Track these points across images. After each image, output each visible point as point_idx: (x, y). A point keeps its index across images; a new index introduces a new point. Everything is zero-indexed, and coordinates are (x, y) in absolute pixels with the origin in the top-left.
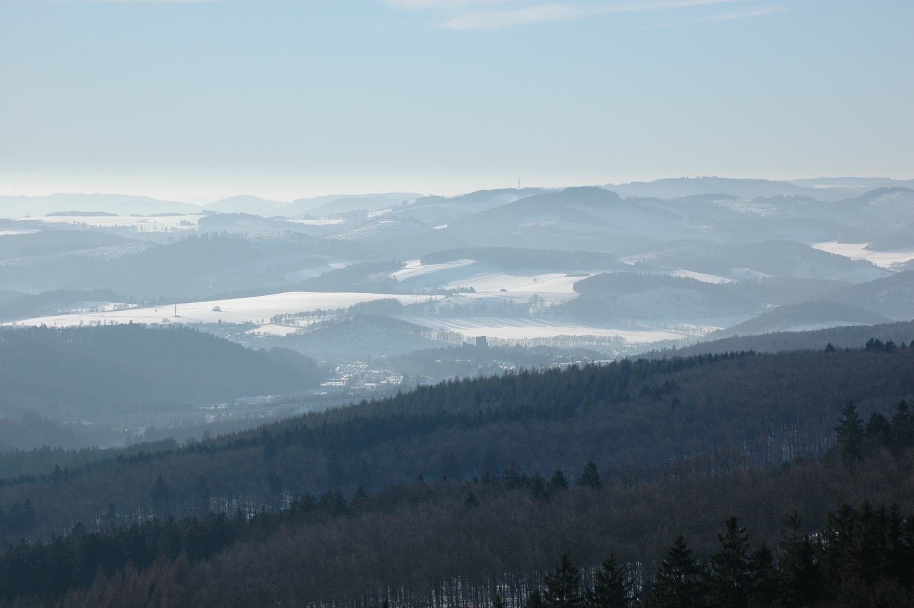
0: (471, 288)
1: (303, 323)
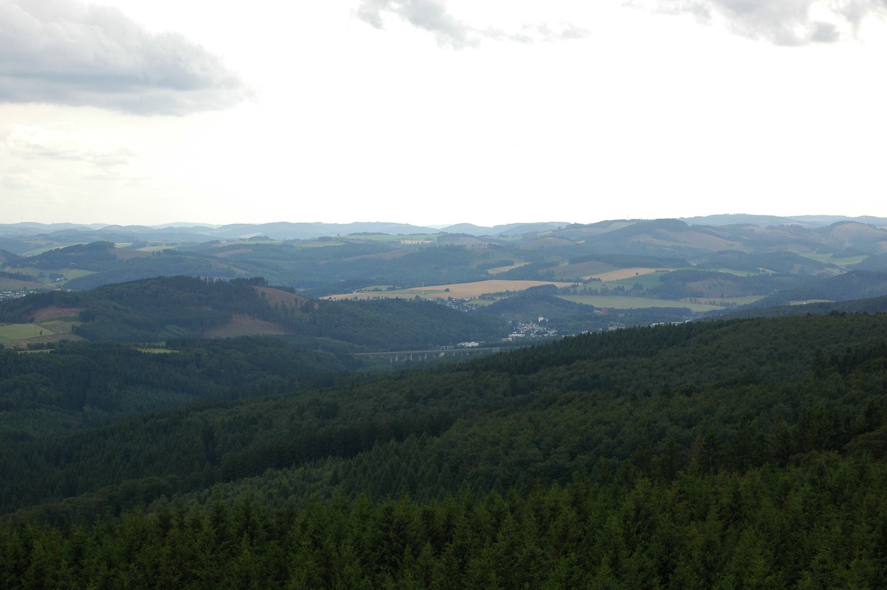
0: (599, 279)
1: (498, 299)
